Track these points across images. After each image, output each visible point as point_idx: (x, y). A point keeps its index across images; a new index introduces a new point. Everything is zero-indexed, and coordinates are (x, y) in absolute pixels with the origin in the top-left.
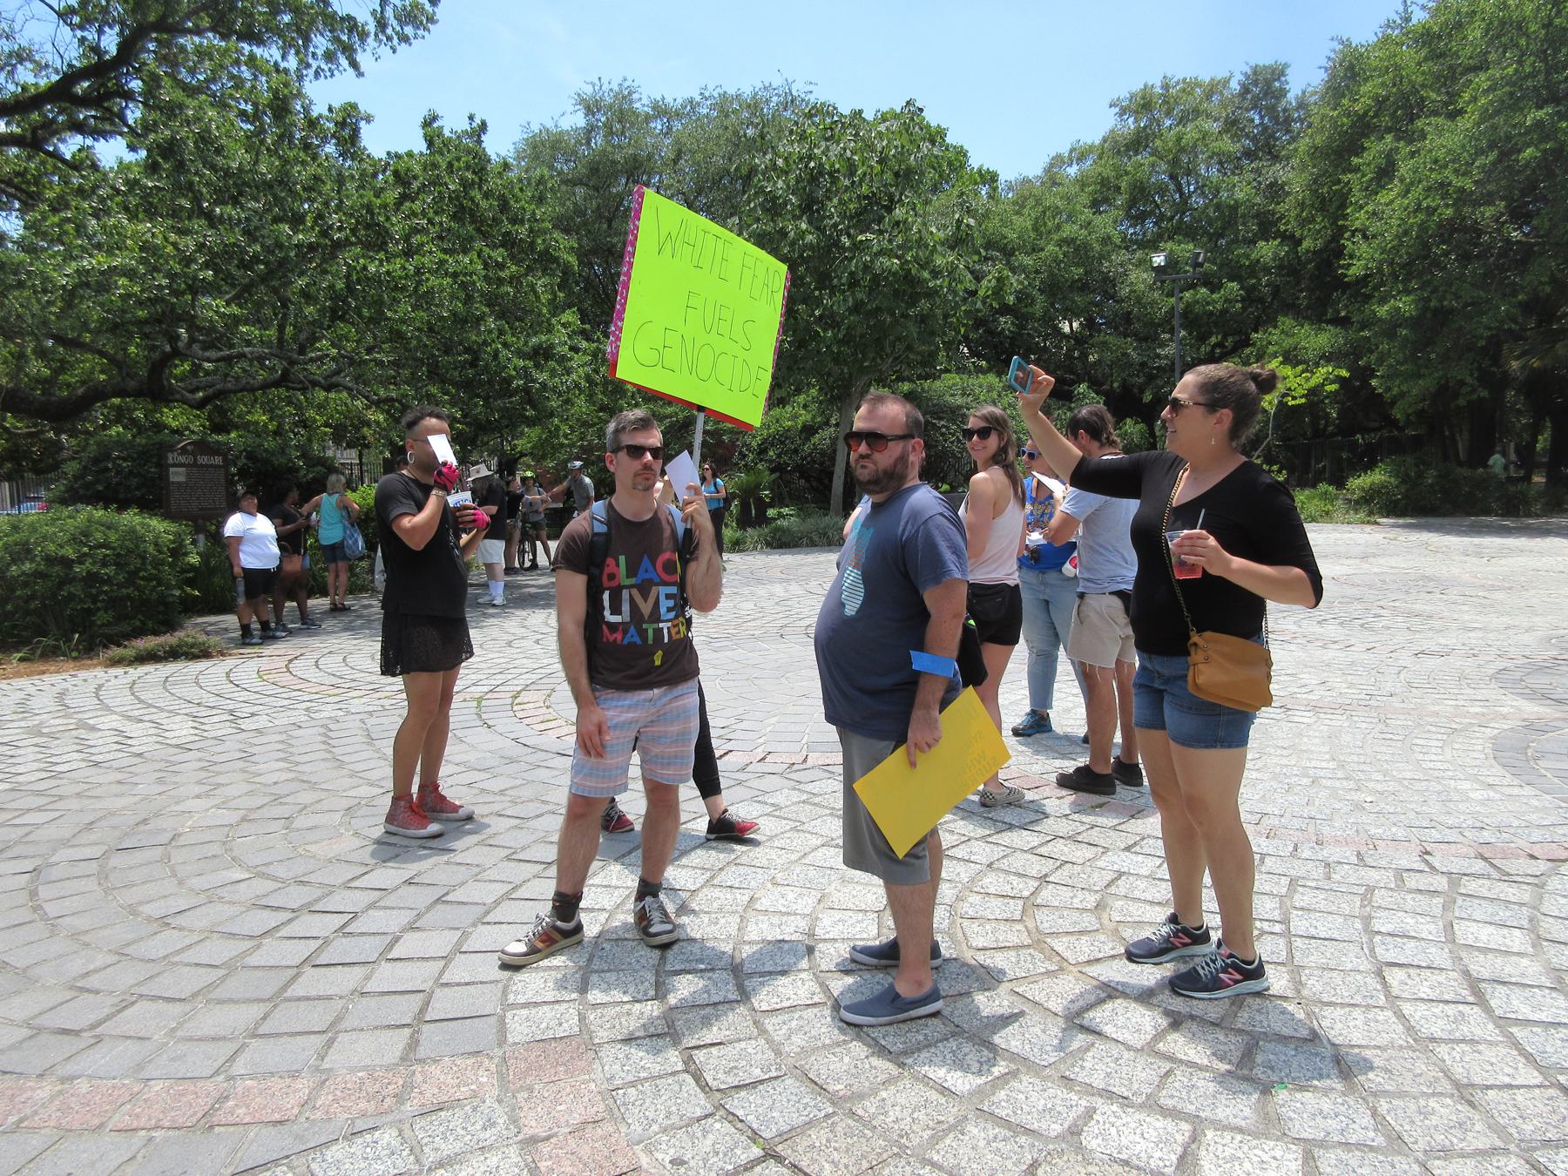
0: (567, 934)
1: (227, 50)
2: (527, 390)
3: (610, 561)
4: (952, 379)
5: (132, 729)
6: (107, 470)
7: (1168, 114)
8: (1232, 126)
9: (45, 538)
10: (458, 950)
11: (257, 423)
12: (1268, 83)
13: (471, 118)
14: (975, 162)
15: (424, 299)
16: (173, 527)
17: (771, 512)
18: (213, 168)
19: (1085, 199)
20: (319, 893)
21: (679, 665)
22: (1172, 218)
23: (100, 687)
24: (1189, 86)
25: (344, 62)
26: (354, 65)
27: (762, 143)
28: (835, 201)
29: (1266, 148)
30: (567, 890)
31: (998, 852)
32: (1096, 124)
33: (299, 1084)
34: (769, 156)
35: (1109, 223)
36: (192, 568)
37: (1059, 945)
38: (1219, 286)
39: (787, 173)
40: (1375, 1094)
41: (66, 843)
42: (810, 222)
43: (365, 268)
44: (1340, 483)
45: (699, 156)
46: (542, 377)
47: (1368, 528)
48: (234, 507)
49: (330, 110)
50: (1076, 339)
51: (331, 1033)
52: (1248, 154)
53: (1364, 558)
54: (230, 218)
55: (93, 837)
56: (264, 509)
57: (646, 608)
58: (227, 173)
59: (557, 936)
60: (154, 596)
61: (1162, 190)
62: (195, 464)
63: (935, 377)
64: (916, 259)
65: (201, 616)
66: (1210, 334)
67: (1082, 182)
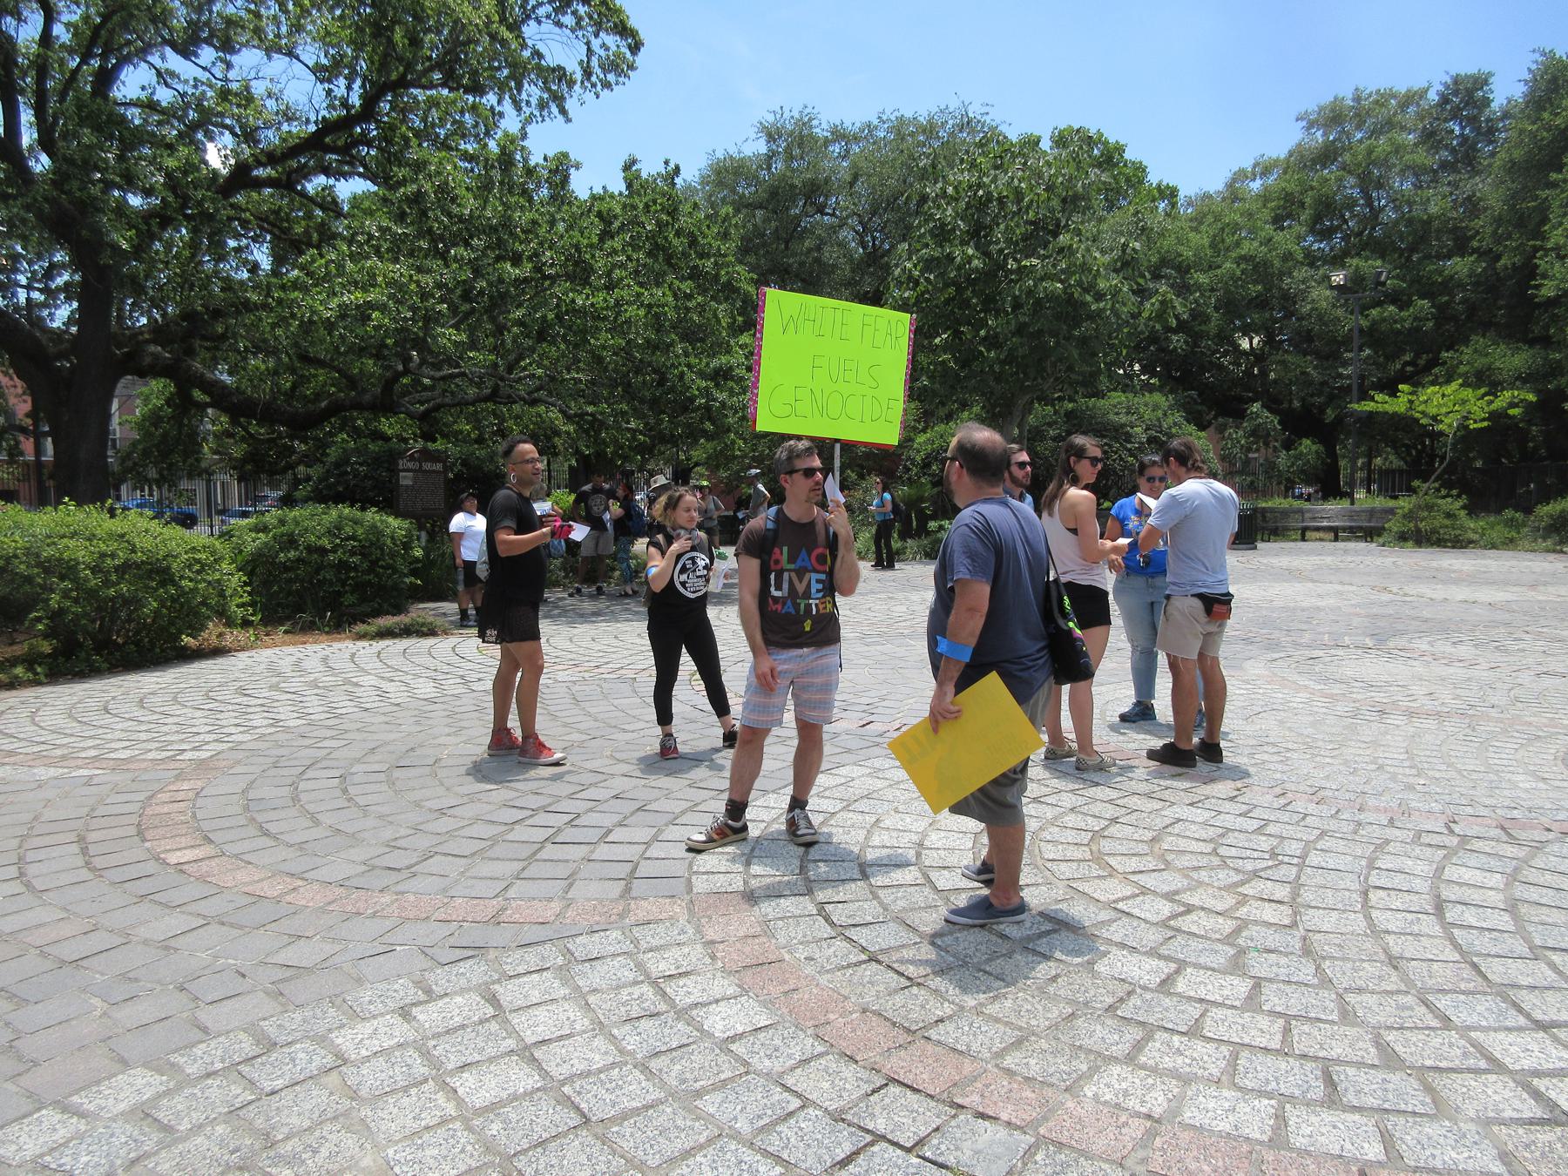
0: (737, 831)
1: (454, 102)
2: (708, 408)
3: (776, 550)
4: (1118, 397)
5: (385, 686)
6: (347, 473)
7: (1359, 127)
8: (1430, 138)
9: (306, 530)
10: (655, 839)
11: (461, 432)
12: (1470, 93)
13: (666, 163)
14: (1153, 178)
15: (618, 328)
16: (406, 524)
17: (932, 525)
18: (449, 215)
19: (1266, 214)
20: (550, 800)
21: (826, 632)
22: (1360, 234)
23: (353, 655)
24: (1382, 99)
25: (554, 109)
26: (563, 112)
27: (932, 173)
28: (1002, 226)
29: (1466, 158)
30: (737, 798)
31: (1081, 801)
32: (1282, 138)
33: (553, 905)
34: (939, 185)
35: (1293, 239)
36: (417, 560)
37: (1112, 861)
38: (1409, 304)
39: (957, 200)
40: (1324, 958)
41: (358, 761)
42: (977, 248)
43: (573, 301)
44: (1528, 511)
45: (875, 180)
46: (722, 396)
47: (1552, 557)
48: (459, 509)
49: (545, 159)
50: (1256, 356)
51: (571, 879)
52: (1444, 165)
53: (1533, 586)
54: (462, 258)
55: (377, 758)
56: (482, 511)
57: (801, 588)
58: (461, 219)
59: (728, 831)
60: (390, 583)
61: (1350, 204)
62: (420, 470)
63: (1099, 395)
64: (1079, 283)
65: (423, 602)
66: (1404, 351)
67: (1265, 197)
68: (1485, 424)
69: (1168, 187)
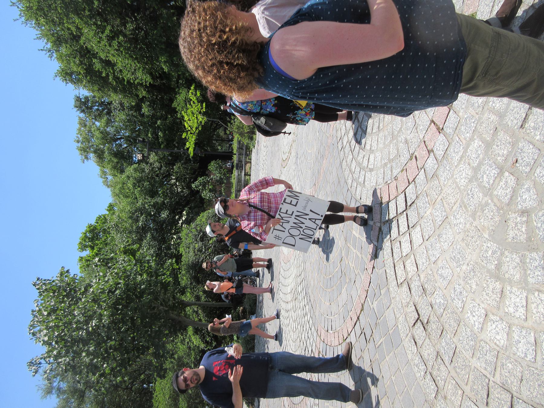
14: (93, 222)
32: (92, 166)
68: (204, 105)
69: (109, 207)
